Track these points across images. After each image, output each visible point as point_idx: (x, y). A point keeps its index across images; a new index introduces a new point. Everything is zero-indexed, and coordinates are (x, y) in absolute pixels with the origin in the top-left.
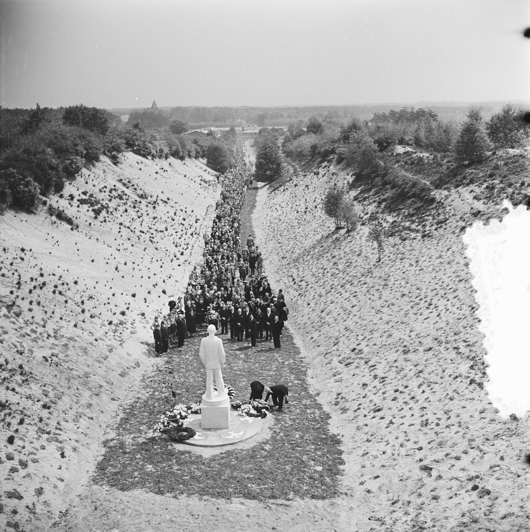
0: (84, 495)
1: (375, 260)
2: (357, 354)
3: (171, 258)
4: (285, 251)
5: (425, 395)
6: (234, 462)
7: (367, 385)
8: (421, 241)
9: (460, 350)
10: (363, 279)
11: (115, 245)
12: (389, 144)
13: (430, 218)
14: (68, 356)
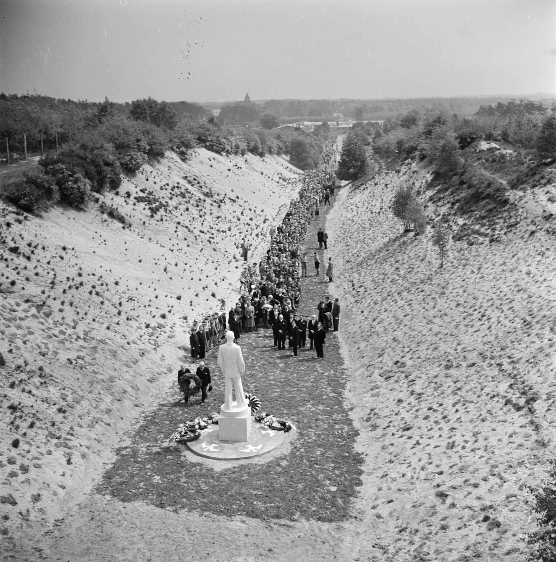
1: (437, 265)
2: (399, 367)
3: (228, 260)
4: (350, 255)
5: (458, 415)
8: (489, 247)
9: (503, 367)
10: (421, 286)
11: (168, 245)
12: (473, 139)
13: (502, 221)
14: (95, 359)
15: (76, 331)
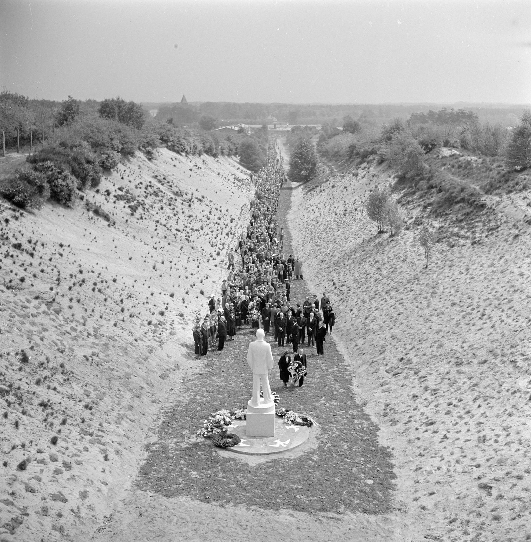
0: (127, 500)
3: (207, 258)
5: (482, 410)
6: (281, 472)
7: (417, 396)
9: (518, 364)
10: (409, 285)
11: (151, 242)
12: (434, 145)
14: (108, 355)
15: (86, 327)
